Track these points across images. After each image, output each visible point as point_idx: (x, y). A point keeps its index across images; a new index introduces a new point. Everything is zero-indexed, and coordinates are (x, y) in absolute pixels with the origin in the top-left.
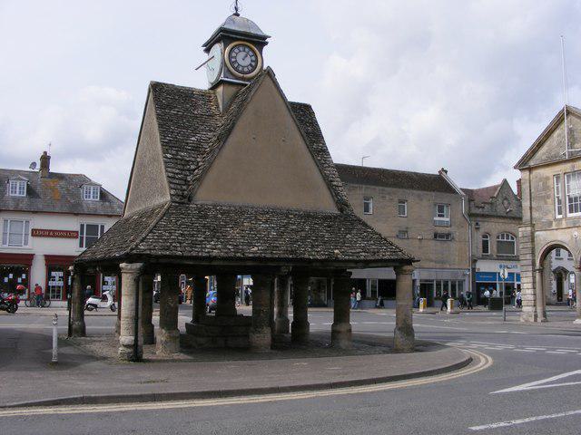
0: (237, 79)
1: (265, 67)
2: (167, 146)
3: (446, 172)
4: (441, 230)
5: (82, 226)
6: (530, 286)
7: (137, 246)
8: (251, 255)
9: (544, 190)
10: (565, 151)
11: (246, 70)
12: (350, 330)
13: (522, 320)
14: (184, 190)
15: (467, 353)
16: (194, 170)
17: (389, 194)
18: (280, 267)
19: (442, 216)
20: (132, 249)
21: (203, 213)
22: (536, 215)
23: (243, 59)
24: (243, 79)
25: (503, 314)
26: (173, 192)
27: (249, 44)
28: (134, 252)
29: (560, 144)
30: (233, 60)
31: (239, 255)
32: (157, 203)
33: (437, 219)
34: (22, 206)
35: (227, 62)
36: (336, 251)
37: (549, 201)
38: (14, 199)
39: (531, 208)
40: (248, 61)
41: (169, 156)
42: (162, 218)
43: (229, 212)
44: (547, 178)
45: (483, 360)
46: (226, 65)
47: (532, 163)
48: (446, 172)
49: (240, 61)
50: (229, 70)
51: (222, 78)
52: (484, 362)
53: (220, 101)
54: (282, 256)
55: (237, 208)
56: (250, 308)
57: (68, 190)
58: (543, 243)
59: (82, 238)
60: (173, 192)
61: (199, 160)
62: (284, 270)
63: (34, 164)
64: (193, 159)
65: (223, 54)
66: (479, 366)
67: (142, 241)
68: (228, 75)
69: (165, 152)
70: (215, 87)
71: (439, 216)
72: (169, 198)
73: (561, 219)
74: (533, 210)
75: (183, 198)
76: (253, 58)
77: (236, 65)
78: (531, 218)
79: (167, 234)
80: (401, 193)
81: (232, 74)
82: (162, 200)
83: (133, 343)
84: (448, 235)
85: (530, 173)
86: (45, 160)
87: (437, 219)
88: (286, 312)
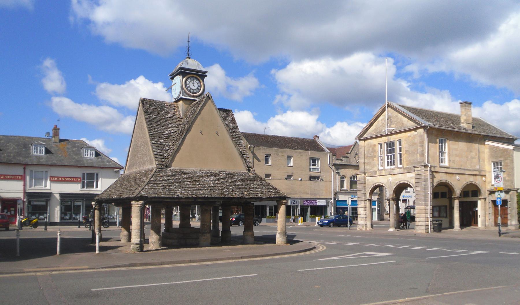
0: (190, 97)
1: (206, 92)
2: (152, 137)
3: (318, 137)
4: (313, 174)
5: (84, 174)
6: (363, 209)
7: (140, 192)
8: (201, 196)
9: (372, 152)
10: (385, 130)
11: (195, 91)
12: (253, 234)
13: (358, 229)
14: (163, 162)
15: (314, 243)
16: (168, 150)
17: (281, 152)
18: (216, 202)
19: (315, 165)
20: (138, 194)
21: (174, 174)
22: (367, 167)
23: (194, 85)
24: (193, 96)
25: (31, 212)
26: (157, 163)
27: (195, 76)
28: (139, 195)
29: (383, 125)
30: (188, 86)
31: (194, 196)
32: (147, 168)
33: (312, 167)
34: (43, 161)
35: (185, 89)
36: (246, 193)
37: (375, 159)
38: (37, 157)
39: (364, 163)
40: (196, 86)
41: (153, 142)
42: (152, 177)
43: (188, 173)
44: (375, 145)
45: (321, 248)
46: (183, 89)
47: (365, 136)
48: (318, 137)
49: (191, 86)
50: (185, 92)
51: (181, 96)
52: (321, 248)
53: (180, 110)
54: (217, 196)
55: (192, 171)
56: (200, 223)
57: (73, 151)
58: (372, 184)
59: (83, 182)
60: (157, 163)
61: (170, 144)
62: (218, 204)
63: (48, 133)
64: (167, 144)
65: (181, 82)
66: (319, 250)
67: (142, 190)
68: (185, 94)
69: (152, 140)
70: (177, 101)
71: (313, 165)
72: (155, 166)
73: (382, 170)
74: (366, 165)
75: (164, 166)
76: (199, 84)
77: (189, 89)
78: (364, 170)
79: (155, 186)
80: (289, 152)
81: (187, 94)
82: (151, 167)
83: (139, 242)
84: (318, 178)
85: (365, 141)
86: (56, 130)
87: (312, 167)
88: (218, 226)
